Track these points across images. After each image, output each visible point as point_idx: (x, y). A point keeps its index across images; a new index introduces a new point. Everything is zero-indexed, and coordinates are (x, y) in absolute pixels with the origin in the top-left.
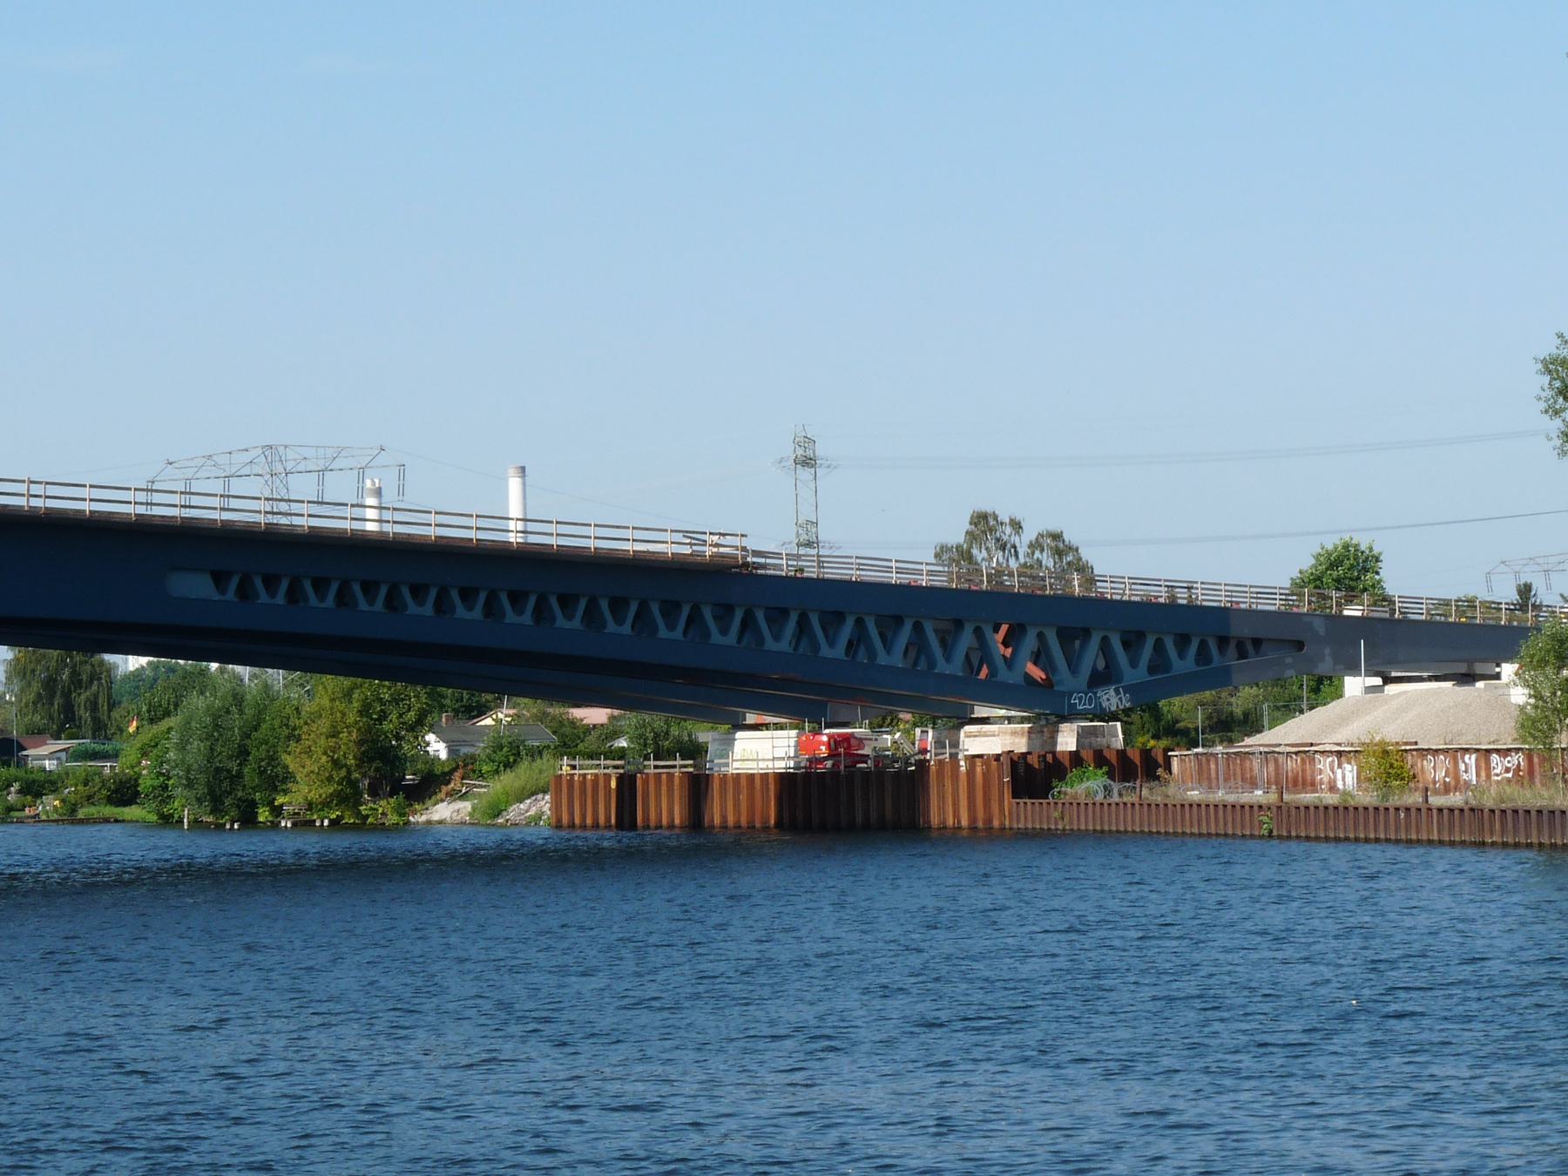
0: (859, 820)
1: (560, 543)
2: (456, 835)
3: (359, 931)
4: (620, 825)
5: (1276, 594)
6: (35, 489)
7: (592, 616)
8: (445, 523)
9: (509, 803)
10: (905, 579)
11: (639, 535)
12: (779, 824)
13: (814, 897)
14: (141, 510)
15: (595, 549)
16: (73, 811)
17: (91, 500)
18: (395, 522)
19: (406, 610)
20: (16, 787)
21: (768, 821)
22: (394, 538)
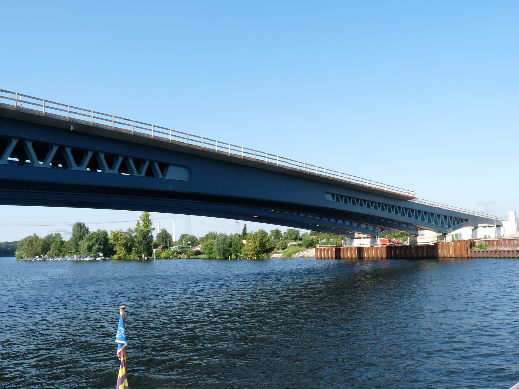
0: (342, 257)
1: (173, 139)
2: (18, 271)
3: (281, 283)
4: (336, 258)
5: (66, 111)
6: (307, 166)
7: (94, 164)
8: (123, 120)
9: (293, 254)
10: (66, 120)
11: (219, 144)
12: (387, 258)
13: (30, 299)
14: (291, 166)
15: (231, 154)
16: (189, 257)
17: (309, 169)
18: (189, 139)
19: (159, 177)
20: (176, 252)
21: (356, 256)
22: (188, 146)
